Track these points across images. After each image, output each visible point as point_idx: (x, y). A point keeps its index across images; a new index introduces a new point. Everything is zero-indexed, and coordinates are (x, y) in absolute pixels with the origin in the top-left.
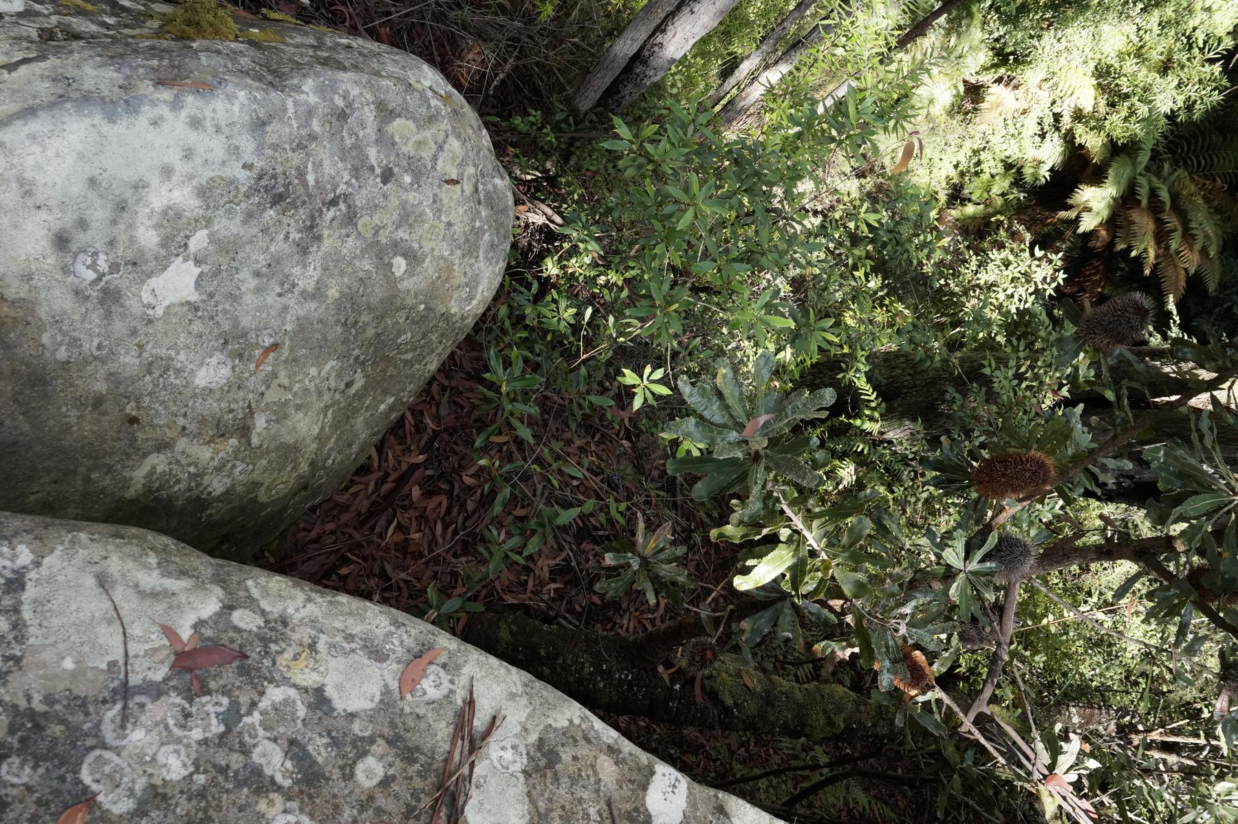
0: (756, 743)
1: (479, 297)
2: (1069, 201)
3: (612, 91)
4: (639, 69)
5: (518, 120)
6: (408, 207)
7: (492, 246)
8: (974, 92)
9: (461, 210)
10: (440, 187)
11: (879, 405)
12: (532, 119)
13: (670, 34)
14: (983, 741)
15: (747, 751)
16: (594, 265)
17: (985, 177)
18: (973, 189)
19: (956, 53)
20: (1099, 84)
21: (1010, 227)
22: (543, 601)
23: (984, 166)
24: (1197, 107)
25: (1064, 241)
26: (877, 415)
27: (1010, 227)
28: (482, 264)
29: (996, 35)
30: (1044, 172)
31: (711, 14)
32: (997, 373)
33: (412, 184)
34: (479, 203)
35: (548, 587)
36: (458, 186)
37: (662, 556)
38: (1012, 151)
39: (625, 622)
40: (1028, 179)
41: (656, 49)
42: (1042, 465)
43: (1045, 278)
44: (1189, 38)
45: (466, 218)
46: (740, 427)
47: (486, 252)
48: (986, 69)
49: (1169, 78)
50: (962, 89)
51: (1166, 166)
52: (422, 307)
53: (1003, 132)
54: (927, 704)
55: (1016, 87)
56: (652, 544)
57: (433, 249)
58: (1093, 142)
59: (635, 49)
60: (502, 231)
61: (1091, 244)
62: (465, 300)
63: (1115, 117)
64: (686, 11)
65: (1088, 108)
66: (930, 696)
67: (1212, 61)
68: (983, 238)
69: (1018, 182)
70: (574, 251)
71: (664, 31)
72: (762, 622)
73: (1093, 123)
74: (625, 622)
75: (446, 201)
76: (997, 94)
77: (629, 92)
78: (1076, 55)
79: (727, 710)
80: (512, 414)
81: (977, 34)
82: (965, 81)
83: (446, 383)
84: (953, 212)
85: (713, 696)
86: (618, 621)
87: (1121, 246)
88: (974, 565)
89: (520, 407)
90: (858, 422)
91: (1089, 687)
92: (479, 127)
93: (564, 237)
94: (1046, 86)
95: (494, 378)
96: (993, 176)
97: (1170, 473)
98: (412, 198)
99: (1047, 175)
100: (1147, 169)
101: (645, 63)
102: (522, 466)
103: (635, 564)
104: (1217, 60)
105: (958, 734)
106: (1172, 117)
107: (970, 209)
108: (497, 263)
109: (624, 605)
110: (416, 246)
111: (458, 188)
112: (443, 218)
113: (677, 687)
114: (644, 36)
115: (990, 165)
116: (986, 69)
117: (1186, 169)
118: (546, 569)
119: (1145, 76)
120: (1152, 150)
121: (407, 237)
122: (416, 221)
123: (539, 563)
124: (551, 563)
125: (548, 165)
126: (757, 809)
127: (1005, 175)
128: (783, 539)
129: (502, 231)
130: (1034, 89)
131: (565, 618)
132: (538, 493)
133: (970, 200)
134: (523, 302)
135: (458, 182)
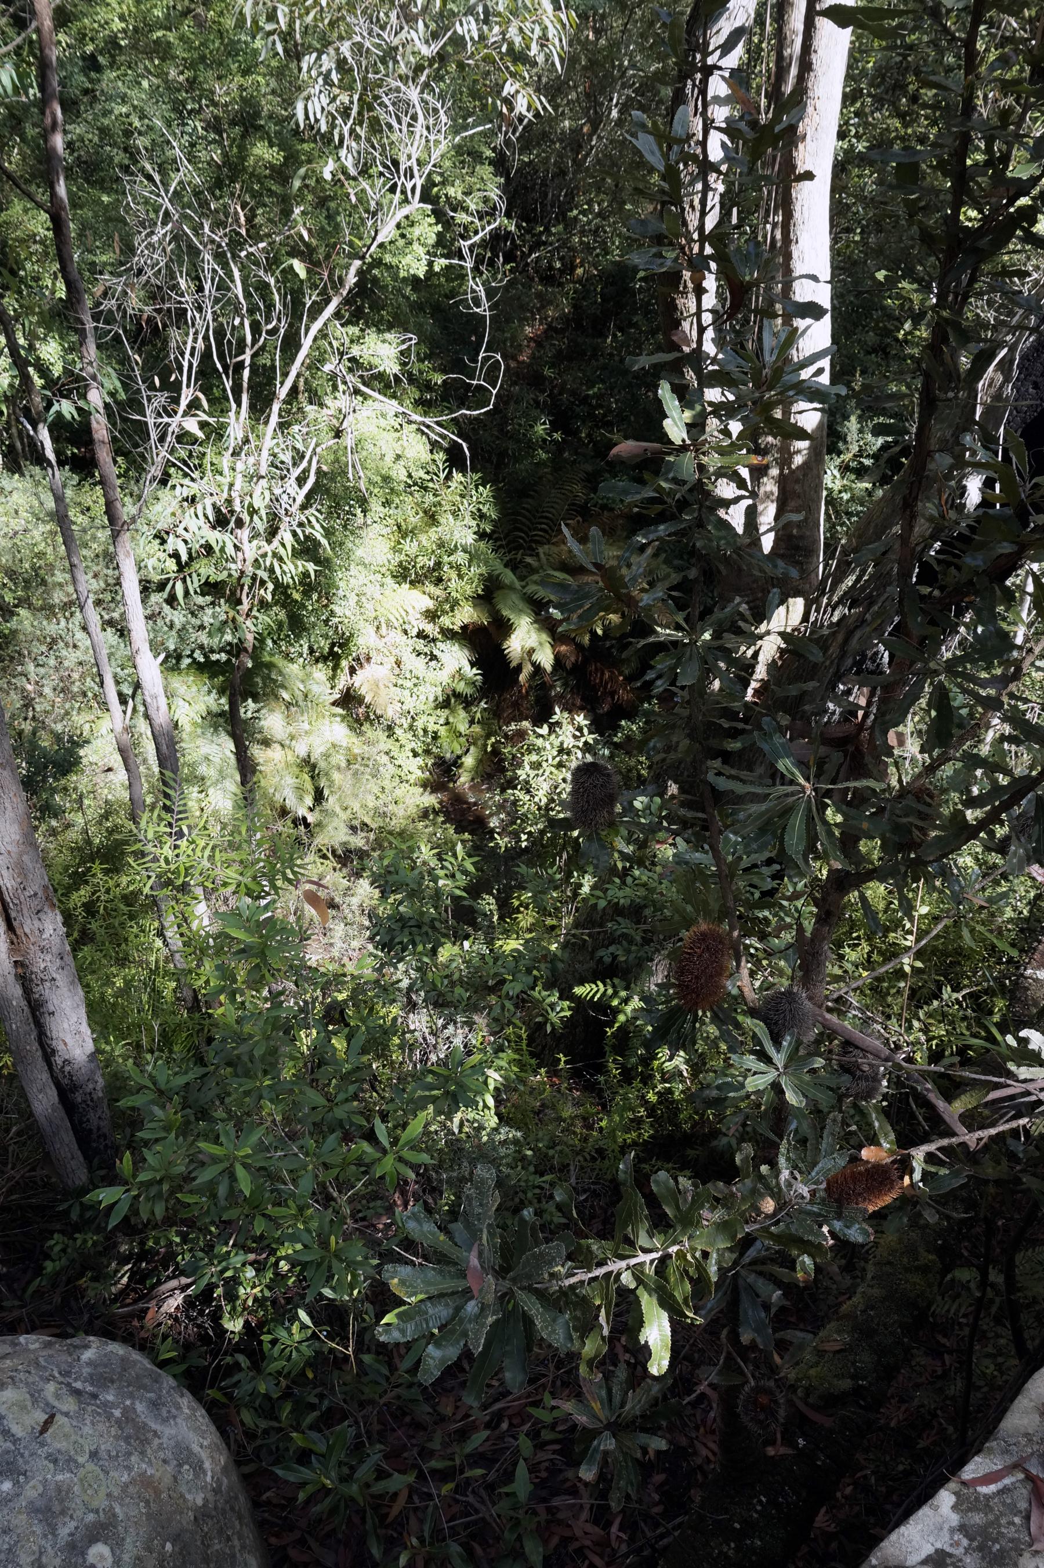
0: (945, 1336)
1: (204, 1455)
2: (514, 664)
3: (84, 1137)
4: (78, 1097)
5: (49, 1266)
6: (39, 1504)
7: (155, 1405)
8: (349, 700)
9: (87, 1430)
10: (42, 1445)
11: (614, 986)
12: (57, 1248)
13: (61, 1047)
14: (993, 1131)
15: (950, 1352)
16: (259, 1267)
17: (443, 731)
18: (449, 748)
19: (300, 698)
20: (412, 583)
21: (506, 736)
22: (626, 1556)
23: (431, 727)
24: (485, 510)
25: (554, 687)
26: (623, 994)
27: (506, 736)
28: (168, 1431)
29: (305, 650)
30: (471, 672)
31: (67, 994)
32: (610, 893)
33: (16, 1483)
34: (95, 1396)
35: (613, 1537)
36: (58, 1417)
37: (617, 1399)
38: (431, 692)
39: (704, 1452)
40: (469, 691)
41: (67, 1069)
42: (703, 937)
43: (575, 737)
44: (415, 484)
45: (101, 1427)
46: (467, 1294)
47: (158, 1417)
48: (333, 678)
49: (442, 520)
50: (339, 711)
51: (529, 560)
52: (169, 1546)
53: (407, 693)
54: (926, 1176)
55: (368, 659)
56: (596, 1406)
57: (109, 1495)
58: (466, 615)
59: (53, 1093)
60: (147, 1381)
61: (569, 665)
62: (196, 1476)
63: (453, 585)
64: (47, 1020)
65: (430, 604)
66: (918, 1164)
67: (449, 477)
68: (503, 770)
69: (467, 702)
70: (233, 1284)
71: (54, 1052)
72: (750, 1312)
73: (447, 607)
74: (704, 1452)
75: (62, 1445)
76: (363, 681)
77: (98, 1119)
78: (373, 590)
79: (857, 1392)
80: (368, 1486)
81: (294, 669)
82: (333, 704)
83: (296, 1535)
84: (462, 779)
85: (831, 1401)
86: (699, 1461)
87: (586, 639)
88: (779, 1059)
89: (365, 1471)
90: (622, 1018)
91: (1027, 920)
92: (14, 1344)
93: (211, 1288)
94: (384, 630)
95: (310, 1489)
96: (447, 723)
97: (756, 840)
98: (32, 1492)
99: (475, 671)
100: (521, 578)
101: (75, 1087)
102: (436, 1507)
103: (608, 1443)
104: (450, 473)
105: (976, 1152)
106: (481, 535)
107: (469, 761)
108: (179, 1408)
109: (684, 1441)
110: (91, 1517)
111: (60, 1419)
112: (81, 1460)
113: (801, 1441)
114: (45, 1076)
115: (433, 722)
116: (333, 678)
117: (542, 544)
118: (590, 1528)
119: (428, 538)
120: (506, 566)
121: (73, 1524)
122: (61, 1501)
123: (578, 1533)
124: (585, 1515)
125: (124, 1248)
126: (912, 1520)
127: (453, 711)
128: (632, 1286)
129: (147, 1381)
130: (380, 644)
131: (662, 1536)
132: (477, 1505)
133: (459, 757)
134: (249, 1387)
135: (52, 1416)
